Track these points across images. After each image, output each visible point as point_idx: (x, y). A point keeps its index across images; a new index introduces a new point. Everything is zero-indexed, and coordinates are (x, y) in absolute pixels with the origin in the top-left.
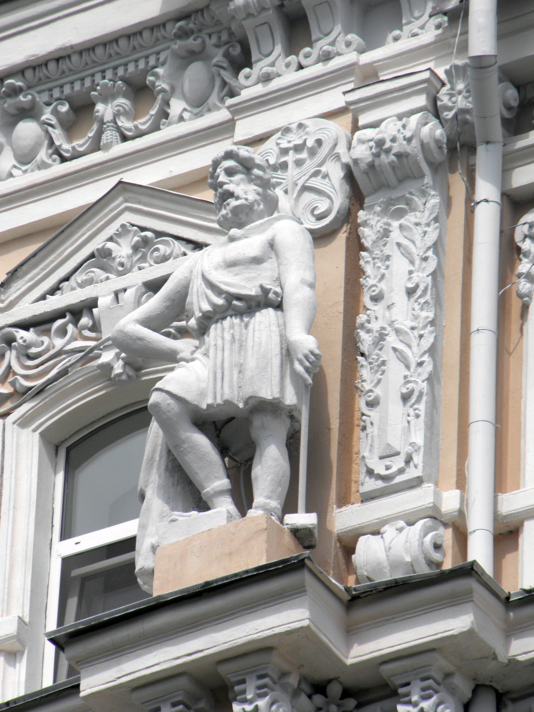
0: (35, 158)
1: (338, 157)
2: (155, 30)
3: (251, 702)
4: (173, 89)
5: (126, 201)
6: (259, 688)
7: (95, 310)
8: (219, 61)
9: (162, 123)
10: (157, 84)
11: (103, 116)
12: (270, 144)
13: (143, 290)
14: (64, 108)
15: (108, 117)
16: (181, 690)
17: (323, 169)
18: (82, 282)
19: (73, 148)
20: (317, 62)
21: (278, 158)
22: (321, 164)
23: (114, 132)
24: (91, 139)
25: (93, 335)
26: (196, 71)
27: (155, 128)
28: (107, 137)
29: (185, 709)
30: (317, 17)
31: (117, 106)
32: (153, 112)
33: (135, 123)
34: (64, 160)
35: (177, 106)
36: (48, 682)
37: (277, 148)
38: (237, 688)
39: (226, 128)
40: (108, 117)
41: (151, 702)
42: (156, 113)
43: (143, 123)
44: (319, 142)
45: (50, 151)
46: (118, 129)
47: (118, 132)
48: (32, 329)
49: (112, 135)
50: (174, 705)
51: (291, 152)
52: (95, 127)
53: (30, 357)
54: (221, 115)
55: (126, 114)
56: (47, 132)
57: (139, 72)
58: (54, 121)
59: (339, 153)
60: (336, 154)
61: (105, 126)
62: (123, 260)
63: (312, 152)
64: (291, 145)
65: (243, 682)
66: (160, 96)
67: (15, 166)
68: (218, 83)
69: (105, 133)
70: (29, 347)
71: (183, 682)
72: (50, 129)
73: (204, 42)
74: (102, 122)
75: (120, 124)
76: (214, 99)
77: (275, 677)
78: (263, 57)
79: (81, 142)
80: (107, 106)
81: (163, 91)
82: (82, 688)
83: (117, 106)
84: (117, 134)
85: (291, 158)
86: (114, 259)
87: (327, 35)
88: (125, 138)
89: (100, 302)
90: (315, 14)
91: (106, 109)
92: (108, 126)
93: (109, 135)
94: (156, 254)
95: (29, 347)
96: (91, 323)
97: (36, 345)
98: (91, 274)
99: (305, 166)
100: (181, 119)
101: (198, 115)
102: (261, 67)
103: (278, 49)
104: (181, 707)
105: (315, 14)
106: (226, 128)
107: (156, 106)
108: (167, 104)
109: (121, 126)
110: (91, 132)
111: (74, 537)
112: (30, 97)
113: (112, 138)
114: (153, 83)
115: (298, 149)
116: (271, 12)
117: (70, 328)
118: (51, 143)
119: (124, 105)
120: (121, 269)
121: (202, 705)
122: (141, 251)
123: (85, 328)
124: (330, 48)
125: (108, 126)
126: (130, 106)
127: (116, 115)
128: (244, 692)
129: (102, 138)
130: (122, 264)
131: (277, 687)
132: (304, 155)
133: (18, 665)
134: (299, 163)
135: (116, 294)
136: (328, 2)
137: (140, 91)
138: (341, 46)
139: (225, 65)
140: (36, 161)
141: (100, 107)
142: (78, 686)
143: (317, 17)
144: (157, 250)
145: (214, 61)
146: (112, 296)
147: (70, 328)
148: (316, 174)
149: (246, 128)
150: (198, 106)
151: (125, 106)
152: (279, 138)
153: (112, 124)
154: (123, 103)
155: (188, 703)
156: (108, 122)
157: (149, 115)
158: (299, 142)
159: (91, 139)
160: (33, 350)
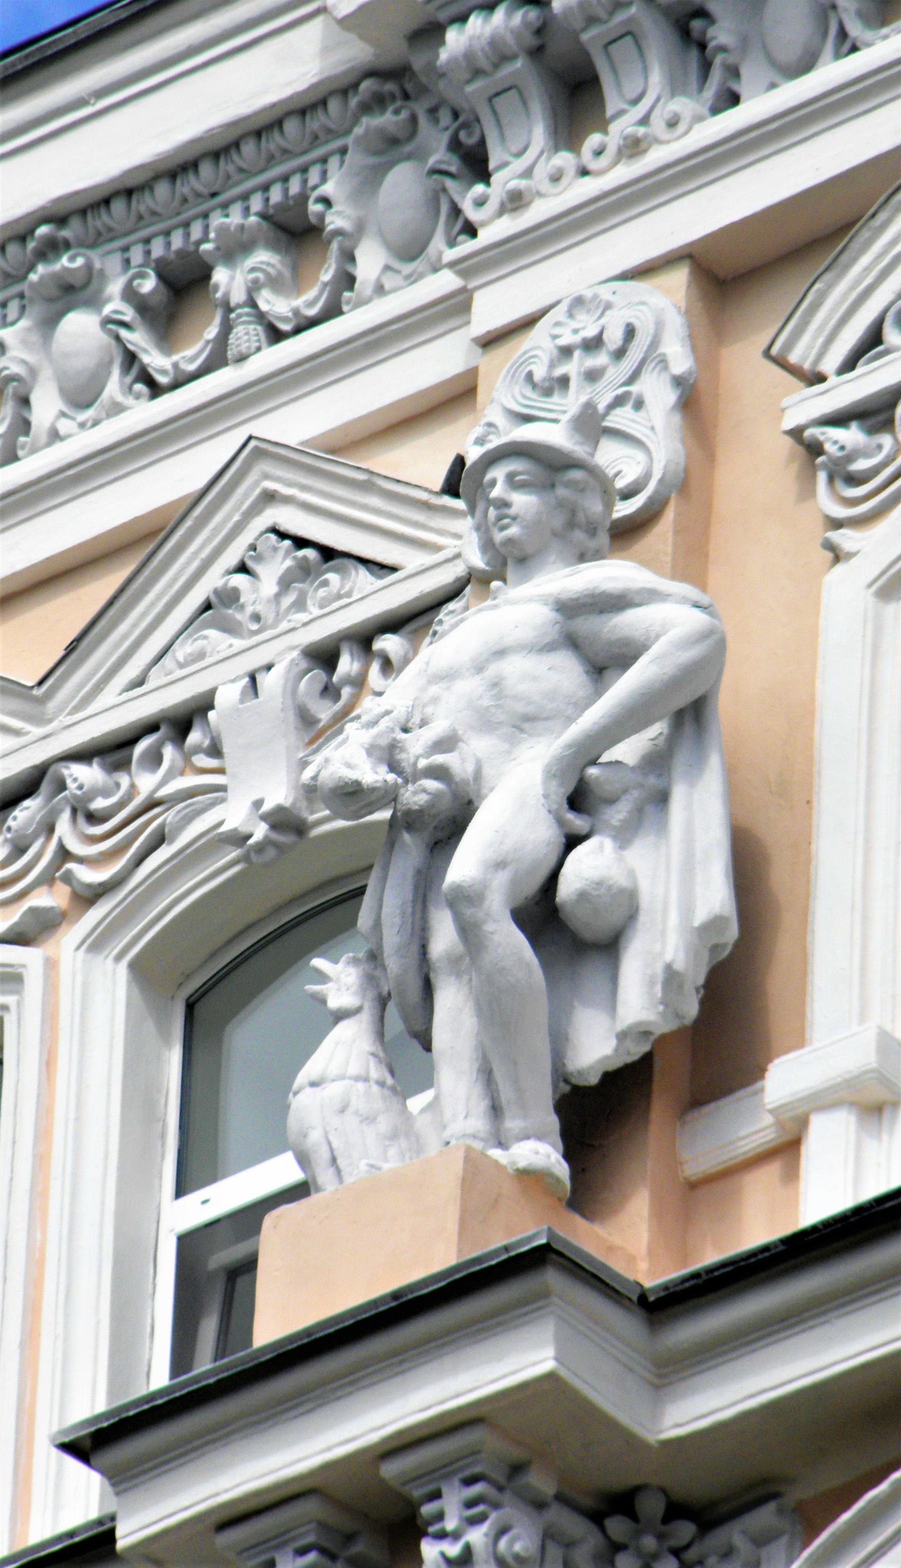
0: (99, 395)
1: (663, 362)
2: (89, 215)
3: (456, 1536)
4: (745, 42)
5: (266, 476)
6: (470, 1504)
7: (211, 715)
8: (440, 162)
9: (343, 299)
10: (328, 219)
11: (227, 295)
12: (538, 336)
13: (304, 665)
14: (148, 285)
15: (238, 296)
16: (310, 1522)
17: (634, 389)
18: (185, 659)
19: (175, 365)
20: (502, 210)
21: (552, 365)
22: (633, 378)
23: (252, 327)
24: (328, 288)
25: (213, 763)
26: (403, 183)
27: (332, 311)
28: (237, 339)
29: (325, 1561)
30: (498, 121)
31: (253, 270)
32: (326, 276)
33: (175, 358)
34: (156, 390)
35: (370, 262)
36: (160, 1377)
37: (551, 346)
38: (427, 1510)
39: (456, 306)
40: (238, 296)
41: (262, 1547)
42: (333, 277)
43: (190, 355)
44: (630, 332)
45: (129, 379)
46: (261, 317)
47: (260, 323)
48: (96, 761)
49: (247, 333)
50: (302, 1552)
51: (577, 354)
52: (217, 320)
53: (854, 480)
54: (445, 282)
55: (275, 283)
56: (118, 338)
57: (172, 256)
58: (129, 314)
59: (664, 355)
60: (660, 355)
61: (233, 315)
62: (259, 608)
63: (620, 354)
64: (577, 339)
65: (436, 1495)
66: (335, 246)
67: (63, 414)
68: (444, 208)
69: (235, 331)
70: (850, 458)
71: (310, 1508)
72: (124, 333)
73: (413, 119)
74: (228, 309)
75: (263, 306)
76: (438, 242)
77: (502, 1480)
78: (511, 159)
79: (189, 352)
80: (235, 271)
81: (338, 232)
82: (119, 1533)
83: (253, 270)
84: (259, 328)
85: (573, 368)
86: (242, 607)
87: (636, 101)
88: (276, 335)
89: (218, 700)
90: (495, 112)
91: (232, 278)
92: (239, 316)
93: (245, 334)
94: (322, 592)
95: (850, 458)
96: (207, 743)
97: (105, 793)
98: (200, 643)
99: (603, 382)
100: (380, 290)
101: (413, 279)
102: (503, 180)
103: (539, 135)
104: (312, 1557)
105: (495, 112)
106: (456, 306)
107: (330, 266)
108: (350, 258)
109: (267, 312)
110: (326, 271)
111: (224, 1176)
112: (80, 262)
113: (249, 340)
114: (321, 217)
115: (594, 344)
116: (519, 64)
117: (169, 752)
118: (130, 358)
119: (264, 267)
120: (255, 627)
121: (359, 1548)
122: (295, 588)
123: (197, 750)
124: (522, 184)
125: (239, 316)
126: (279, 266)
127: (253, 289)
128: (440, 1517)
129: (230, 341)
130: (256, 618)
131: (506, 1497)
132: (601, 359)
133: (885, 1137)
134: (592, 376)
135: (253, 678)
136: (490, 99)
137: (296, 232)
138: (658, 125)
139: (453, 169)
140: (102, 401)
141: (220, 275)
142: (112, 1531)
143: (498, 121)
144: (325, 583)
145: (107, 309)
146: (247, 679)
147: (169, 752)
148: (619, 401)
149: (493, 307)
150: (412, 258)
151: (270, 269)
152: (557, 324)
153: (247, 310)
154: (262, 263)
155: (326, 1544)
156: (239, 306)
157: (319, 283)
158: (591, 332)
159: (328, 288)
160: (861, 465)
